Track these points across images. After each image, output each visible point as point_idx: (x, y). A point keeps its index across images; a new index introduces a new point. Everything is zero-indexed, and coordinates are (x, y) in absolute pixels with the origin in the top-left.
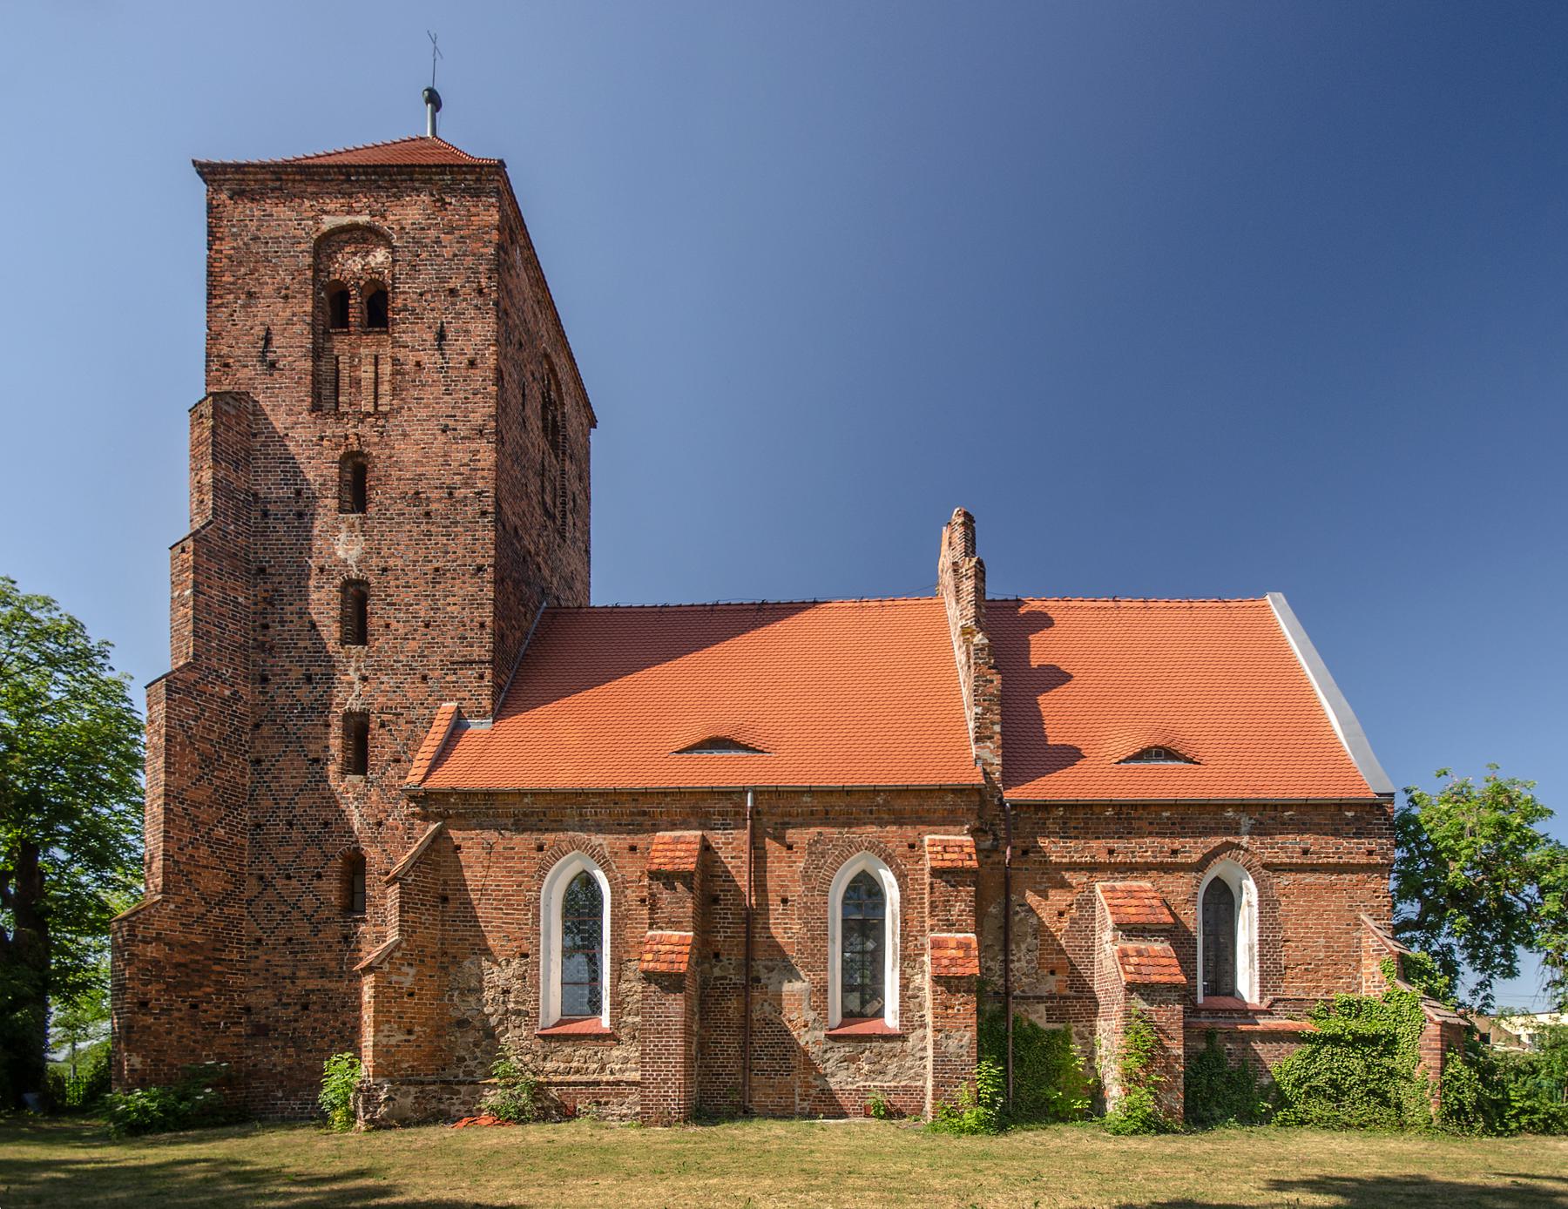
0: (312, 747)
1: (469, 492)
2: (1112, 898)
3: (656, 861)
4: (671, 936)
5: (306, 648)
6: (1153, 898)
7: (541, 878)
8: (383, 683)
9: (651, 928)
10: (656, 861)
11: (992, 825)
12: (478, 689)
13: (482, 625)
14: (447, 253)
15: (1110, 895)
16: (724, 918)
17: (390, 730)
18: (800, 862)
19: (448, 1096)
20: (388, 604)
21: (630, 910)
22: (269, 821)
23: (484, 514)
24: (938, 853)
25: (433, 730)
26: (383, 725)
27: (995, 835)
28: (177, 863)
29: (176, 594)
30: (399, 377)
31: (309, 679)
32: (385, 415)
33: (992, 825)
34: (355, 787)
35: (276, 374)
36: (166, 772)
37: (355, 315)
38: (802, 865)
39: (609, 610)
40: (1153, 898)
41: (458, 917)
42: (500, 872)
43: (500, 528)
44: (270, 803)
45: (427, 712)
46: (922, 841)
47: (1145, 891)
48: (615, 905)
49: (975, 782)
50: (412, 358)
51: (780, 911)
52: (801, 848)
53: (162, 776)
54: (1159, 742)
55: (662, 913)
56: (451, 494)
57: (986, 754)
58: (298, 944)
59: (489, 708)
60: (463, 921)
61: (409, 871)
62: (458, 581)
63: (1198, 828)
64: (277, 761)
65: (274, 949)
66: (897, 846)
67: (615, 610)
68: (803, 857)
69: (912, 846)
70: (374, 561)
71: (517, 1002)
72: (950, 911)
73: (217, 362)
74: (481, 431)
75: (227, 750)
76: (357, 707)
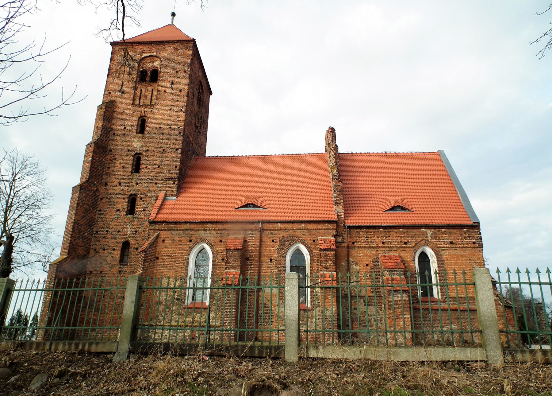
0: (118, 206)
1: (176, 127)
2: (384, 259)
3: (229, 246)
4: (232, 272)
5: (120, 174)
6: (398, 259)
7: (190, 251)
8: (142, 185)
9: (226, 269)
10: (229, 246)
11: (342, 233)
12: (172, 187)
13: (176, 167)
14: (176, 62)
15: (383, 258)
16: (250, 266)
17: (143, 200)
18: (276, 246)
19: (152, 330)
20: (148, 161)
21: (219, 263)
22: (101, 230)
23: (180, 133)
24: (322, 243)
25: (158, 201)
26: (141, 199)
27: (343, 237)
28: (73, 245)
29: (86, 159)
30: (159, 95)
31: (120, 184)
32: (153, 105)
33: (342, 233)
34: (129, 219)
35: (123, 95)
36: (75, 215)
37: (148, 78)
38: (277, 247)
39: (214, 158)
40: (398, 259)
41: (161, 264)
42: (177, 249)
43: (184, 137)
44: (102, 224)
45: (156, 194)
46: (317, 239)
47: (396, 257)
48: (214, 261)
49: (334, 219)
50: (163, 89)
51: (269, 263)
52: (276, 241)
53: (74, 216)
54: (398, 204)
55: (230, 264)
56: (170, 127)
57: (338, 209)
58: (104, 273)
59: (176, 193)
60: (163, 266)
61: (148, 248)
62: (170, 153)
63: (413, 234)
64: (106, 210)
65: (96, 275)
66: (309, 241)
67: (217, 158)
68: (277, 244)
69: (314, 241)
70: (145, 148)
71: (178, 296)
72: (327, 264)
73: (107, 92)
74: (181, 109)
75: (92, 207)
76: (133, 193)
